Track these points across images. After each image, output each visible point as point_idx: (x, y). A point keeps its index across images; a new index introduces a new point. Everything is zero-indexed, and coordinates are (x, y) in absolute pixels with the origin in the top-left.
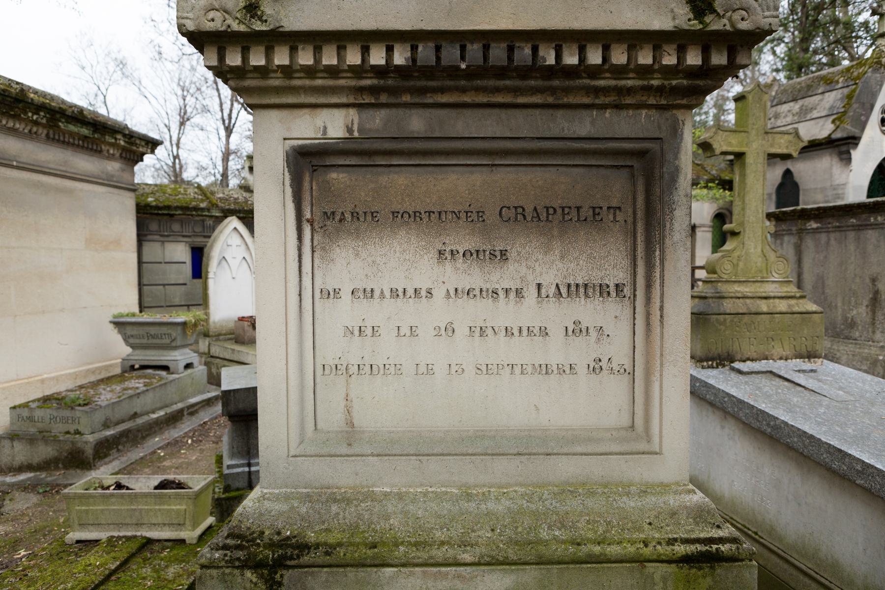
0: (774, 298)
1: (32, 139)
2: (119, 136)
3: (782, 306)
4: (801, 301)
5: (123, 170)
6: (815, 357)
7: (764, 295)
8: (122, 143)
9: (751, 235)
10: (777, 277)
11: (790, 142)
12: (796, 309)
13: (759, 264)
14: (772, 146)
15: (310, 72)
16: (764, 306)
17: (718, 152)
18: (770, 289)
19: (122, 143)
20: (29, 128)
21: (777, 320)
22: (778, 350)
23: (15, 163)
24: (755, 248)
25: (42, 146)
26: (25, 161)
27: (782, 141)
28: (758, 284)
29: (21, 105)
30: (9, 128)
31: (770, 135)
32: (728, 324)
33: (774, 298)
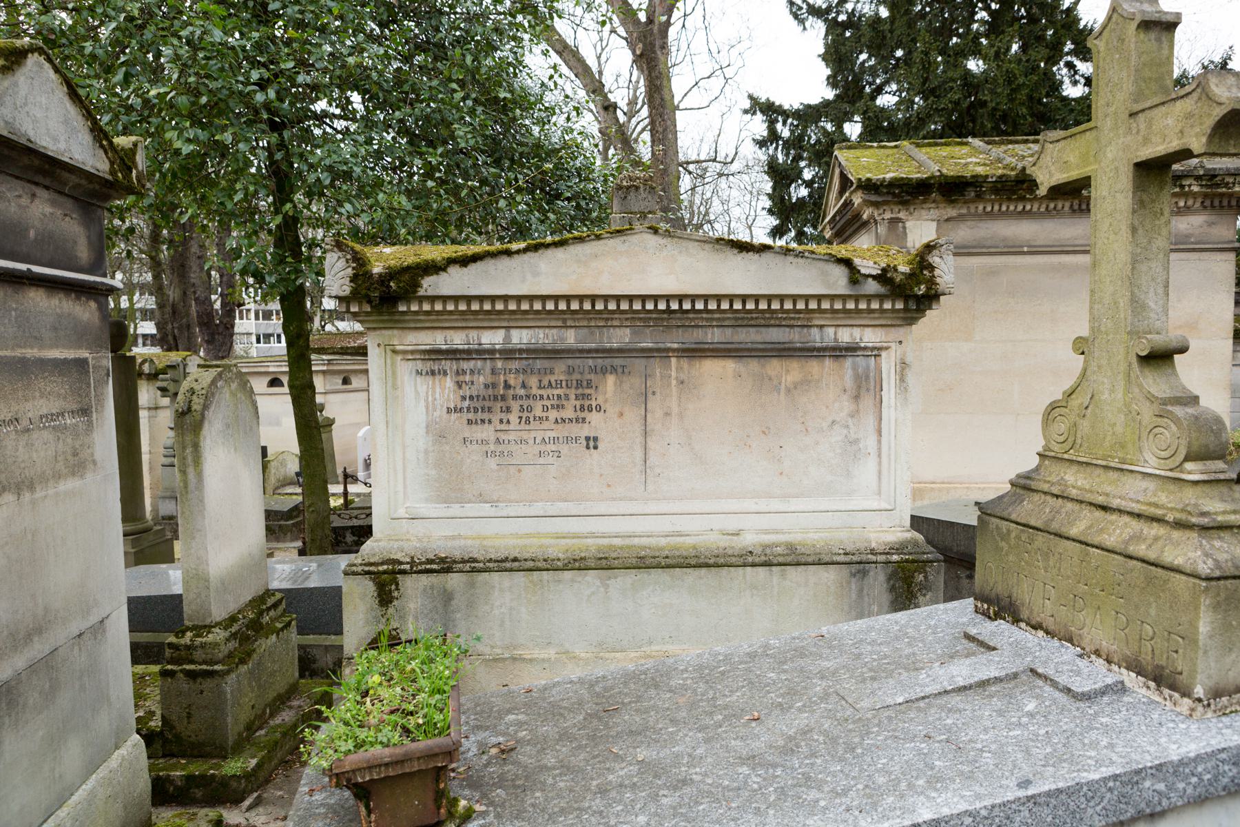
0: (1121, 511)
1: (1053, 217)
2: (1186, 182)
3: (1117, 532)
4: (1176, 534)
5: (1211, 224)
6: (1173, 687)
7: (1100, 500)
8: (1195, 189)
9: (1104, 362)
10: (1152, 465)
11: (1189, 116)
12: (1141, 550)
13: (1119, 429)
14: (1146, 141)
15: (427, 313)
16: (1081, 523)
17: (1042, 191)
18: (1131, 492)
19: (1195, 189)
20: (1044, 206)
21: (1094, 563)
22: (1099, 633)
23: (1025, 249)
24: (1112, 391)
25: (1068, 221)
26: (1042, 243)
27: (1170, 121)
28: (1113, 475)
29: (1025, 186)
30: (1020, 213)
31: (1141, 117)
32: (1013, 542)
33: (1121, 511)
